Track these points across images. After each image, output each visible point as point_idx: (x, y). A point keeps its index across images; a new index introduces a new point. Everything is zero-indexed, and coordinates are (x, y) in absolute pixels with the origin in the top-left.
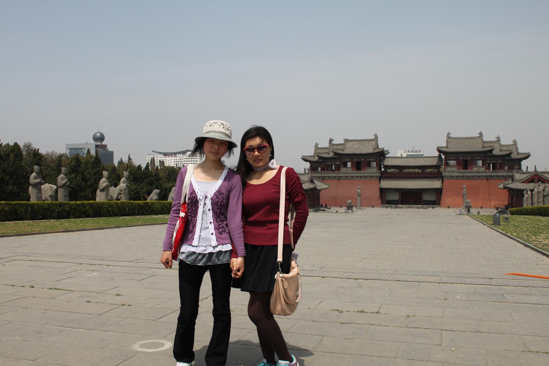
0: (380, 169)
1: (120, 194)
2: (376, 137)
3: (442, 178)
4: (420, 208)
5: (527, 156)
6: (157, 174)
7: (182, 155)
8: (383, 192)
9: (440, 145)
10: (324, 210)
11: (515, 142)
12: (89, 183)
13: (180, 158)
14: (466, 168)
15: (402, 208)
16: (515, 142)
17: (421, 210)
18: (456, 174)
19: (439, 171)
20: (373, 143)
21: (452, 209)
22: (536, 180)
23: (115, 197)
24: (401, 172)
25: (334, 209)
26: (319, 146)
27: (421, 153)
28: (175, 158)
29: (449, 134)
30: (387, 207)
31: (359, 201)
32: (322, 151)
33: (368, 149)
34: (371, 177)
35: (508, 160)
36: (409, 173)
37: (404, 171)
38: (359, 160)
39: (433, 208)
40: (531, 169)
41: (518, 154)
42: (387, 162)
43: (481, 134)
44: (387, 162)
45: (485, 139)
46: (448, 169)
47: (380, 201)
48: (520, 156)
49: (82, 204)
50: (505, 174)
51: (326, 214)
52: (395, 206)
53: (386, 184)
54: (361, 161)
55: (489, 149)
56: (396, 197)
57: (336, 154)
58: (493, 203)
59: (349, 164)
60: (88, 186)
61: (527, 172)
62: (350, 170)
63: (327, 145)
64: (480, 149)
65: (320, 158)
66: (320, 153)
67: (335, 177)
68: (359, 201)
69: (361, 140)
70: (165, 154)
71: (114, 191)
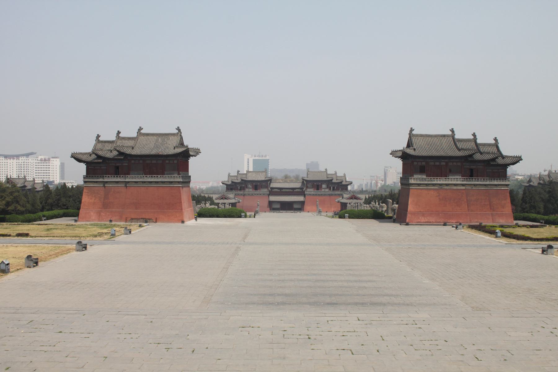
7: (25, 158)
8: (271, 203)
13: (23, 161)
14: (318, 189)
16: (345, 174)
18: (312, 193)
24: (281, 192)
28: (18, 161)
29: (412, 130)
33: (170, 148)
41: (503, 157)
45: (328, 173)
48: (347, 183)
53: (273, 198)
54: (257, 185)
56: (278, 206)
57: (242, 180)
58: (333, 209)
63: (113, 138)
64: (325, 179)
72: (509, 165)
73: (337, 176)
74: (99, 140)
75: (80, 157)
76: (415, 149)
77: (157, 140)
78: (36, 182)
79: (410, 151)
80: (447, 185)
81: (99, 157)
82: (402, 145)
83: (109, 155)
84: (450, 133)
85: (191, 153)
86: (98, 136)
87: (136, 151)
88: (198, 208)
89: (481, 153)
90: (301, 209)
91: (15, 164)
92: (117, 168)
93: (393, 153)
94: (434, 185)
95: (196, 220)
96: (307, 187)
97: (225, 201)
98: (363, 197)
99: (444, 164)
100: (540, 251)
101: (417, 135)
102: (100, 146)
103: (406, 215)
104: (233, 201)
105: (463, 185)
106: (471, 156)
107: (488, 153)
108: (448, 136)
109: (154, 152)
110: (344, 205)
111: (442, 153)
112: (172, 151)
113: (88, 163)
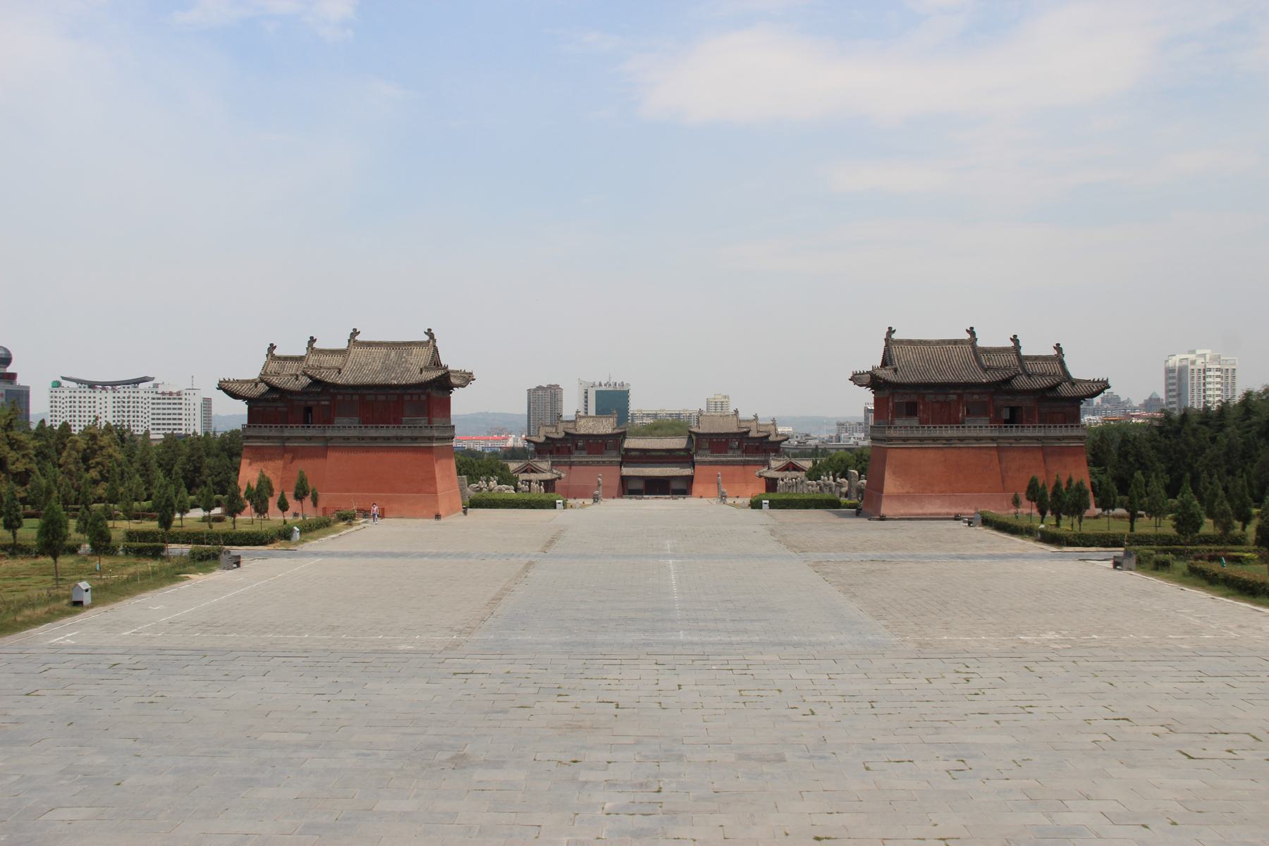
8: (624, 480)
24: (647, 457)
28: (117, 395)
29: (891, 331)
33: (414, 372)
41: (1074, 383)
43: (971, 332)
45: (981, 343)
48: (779, 439)
53: (627, 471)
56: (640, 485)
57: (567, 434)
63: (302, 351)
64: (735, 430)
72: (1083, 398)
73: (758, 425)
74: (273, 355)
75: (235, 387)
76: (896, 370)
77: (388, 355)
78: (152, 437)
79: (887, 374)
80: (961, 439)
81: (273, 388)
82: (871, 360)
83: (293, 385)
84: (967, 336)
85: (453, 380)
86: (272, 347)
87: (347, 378)
88: (470, 491)
89: (1029, 376)
91: (110, 400)
92: (309, 410)
93: (856, 379)
94: (935, 439)
95: (465, 513)
96: (698, 448)
97: (533, 476)
98: (807, 464)
99: (954, 397)
100: (1109, 564)
101: (901, 342)
102: (274, 366)
103: (879, 500)
104: (548, 476)
105: (993, 439)
106: (1007, 381)
107: (1042, 375)
108: (962, 342)
109: (380, 379)
110: (771, 485)
111: (950, 377)
112: (415, 377)
113: (250, 401)
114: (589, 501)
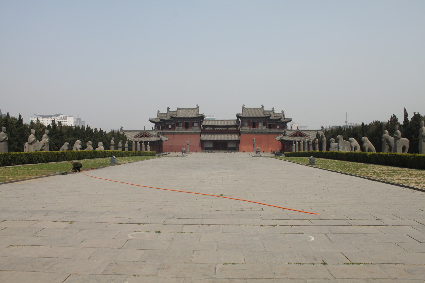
0: (200, 127)
1: (44, 146)
2: (198, 107)
3: (240, 134)
4: (226, 152)
5: (290, 120)
6: (61, 132)
8: (202, 142)
9: (238, 113)
10: (166, 155)
11: (283, 111)
12: (15, 138)
14: (254, 127)
15: (215, 152)
16: (283, 111)
17: (227, 154)
19: (237, 129)
20: (196, 110)
21: (246, 153)
22: (298, 135)
23: (40, 148)
24: (214, 129)
25: (172, 154)
26: (160, 112)
27: (214, 117)
29: (243, 106)
30: (205, 152)
31: (188, 149)
32: (162, 115)
34: (195, 133)
35: (279, 122)
36: (218, 130)
37: (215, 129)
38: (187, 122)
39: (235, 152)
40: (295, 128)
41: (285, 119)
42: (204, 123)
43: (263, 106)
44: (204, 123)
45: (265, 109)
46: (244, 128)
47: (201, 148)
48: (286, 120)
49: (20, 154)
50: (277, 131)
51: (167, 158)
52: (210, 151)
53: (205, 137)
55: (268, 115)
56: (211, 146)
57: (172, 117)
58: (270, 149)
59: (181, 124)
60: (14, 140)
61: (291, 130)
62: (181, 128)
65: (161, 120)
66: (161, 117)
67: (171, 133)
68: (188, 149)
69: (188, 109)
70: (44, 117)
71: (39, 144)
90: (235, 149)
104: (155, 139)
114: (180, 154)
